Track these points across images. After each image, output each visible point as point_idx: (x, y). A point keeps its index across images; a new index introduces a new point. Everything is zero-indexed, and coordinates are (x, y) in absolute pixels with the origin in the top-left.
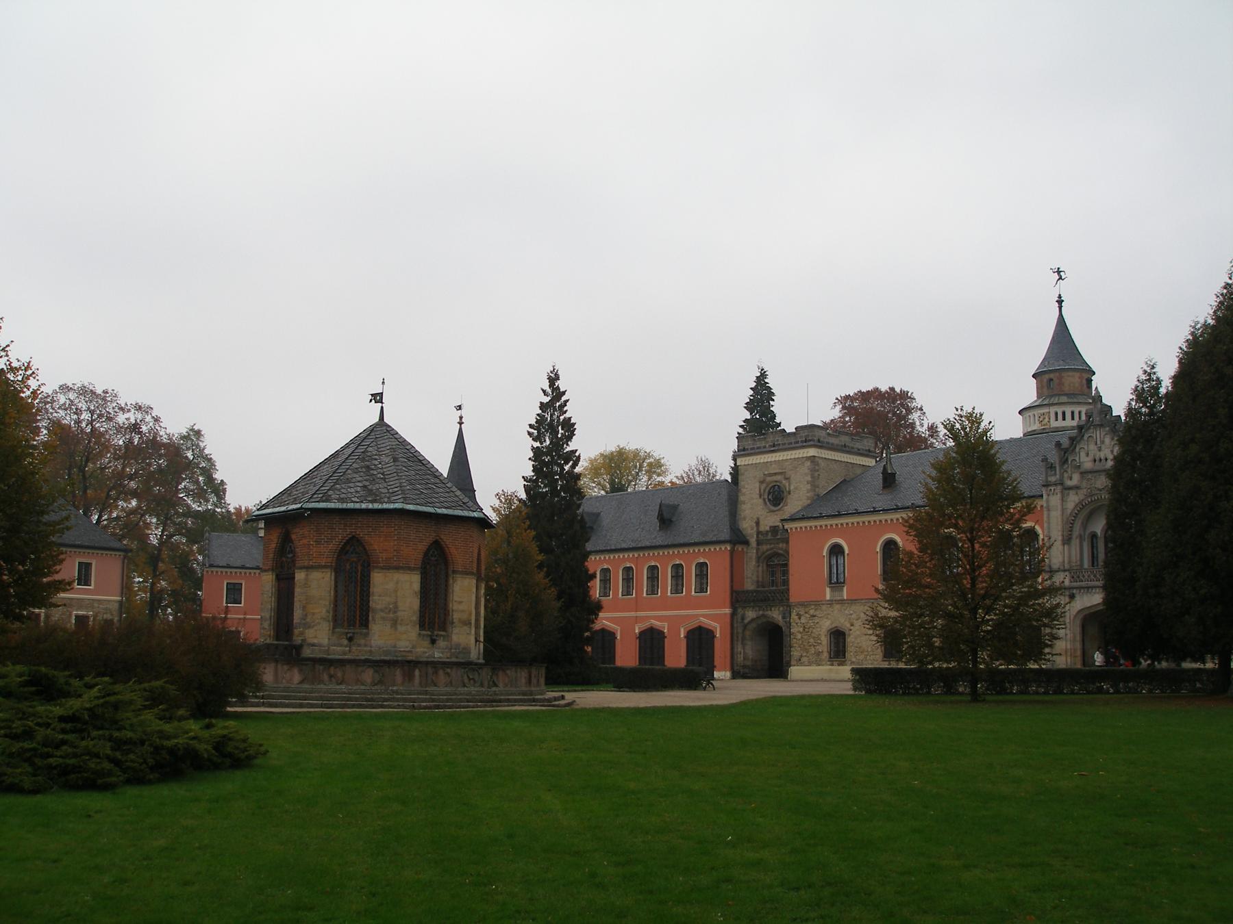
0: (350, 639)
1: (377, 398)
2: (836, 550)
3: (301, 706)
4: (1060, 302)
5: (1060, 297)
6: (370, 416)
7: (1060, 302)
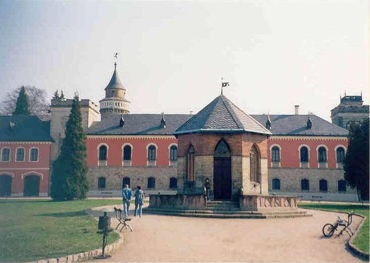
0: (255, 186)
2: (103, 148)
3: (204, 213)
4: (115, 65)
5: (116, 63)
7: (115, 65)
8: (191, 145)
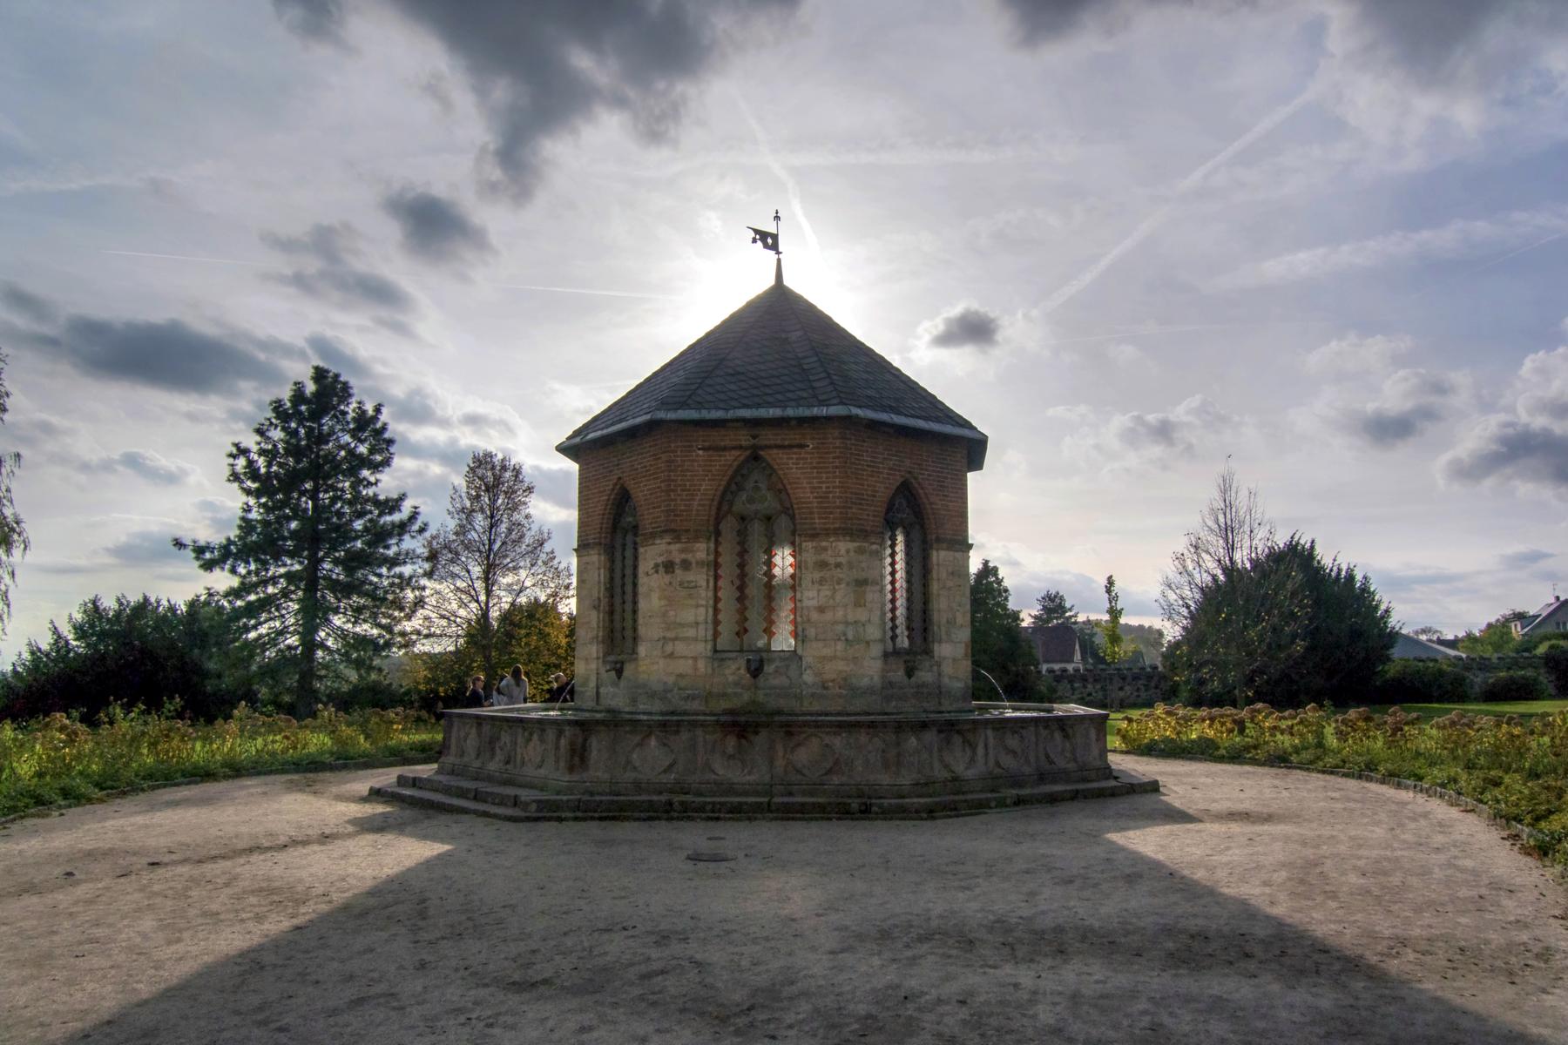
1: (768, 240)
8: (622, 500)
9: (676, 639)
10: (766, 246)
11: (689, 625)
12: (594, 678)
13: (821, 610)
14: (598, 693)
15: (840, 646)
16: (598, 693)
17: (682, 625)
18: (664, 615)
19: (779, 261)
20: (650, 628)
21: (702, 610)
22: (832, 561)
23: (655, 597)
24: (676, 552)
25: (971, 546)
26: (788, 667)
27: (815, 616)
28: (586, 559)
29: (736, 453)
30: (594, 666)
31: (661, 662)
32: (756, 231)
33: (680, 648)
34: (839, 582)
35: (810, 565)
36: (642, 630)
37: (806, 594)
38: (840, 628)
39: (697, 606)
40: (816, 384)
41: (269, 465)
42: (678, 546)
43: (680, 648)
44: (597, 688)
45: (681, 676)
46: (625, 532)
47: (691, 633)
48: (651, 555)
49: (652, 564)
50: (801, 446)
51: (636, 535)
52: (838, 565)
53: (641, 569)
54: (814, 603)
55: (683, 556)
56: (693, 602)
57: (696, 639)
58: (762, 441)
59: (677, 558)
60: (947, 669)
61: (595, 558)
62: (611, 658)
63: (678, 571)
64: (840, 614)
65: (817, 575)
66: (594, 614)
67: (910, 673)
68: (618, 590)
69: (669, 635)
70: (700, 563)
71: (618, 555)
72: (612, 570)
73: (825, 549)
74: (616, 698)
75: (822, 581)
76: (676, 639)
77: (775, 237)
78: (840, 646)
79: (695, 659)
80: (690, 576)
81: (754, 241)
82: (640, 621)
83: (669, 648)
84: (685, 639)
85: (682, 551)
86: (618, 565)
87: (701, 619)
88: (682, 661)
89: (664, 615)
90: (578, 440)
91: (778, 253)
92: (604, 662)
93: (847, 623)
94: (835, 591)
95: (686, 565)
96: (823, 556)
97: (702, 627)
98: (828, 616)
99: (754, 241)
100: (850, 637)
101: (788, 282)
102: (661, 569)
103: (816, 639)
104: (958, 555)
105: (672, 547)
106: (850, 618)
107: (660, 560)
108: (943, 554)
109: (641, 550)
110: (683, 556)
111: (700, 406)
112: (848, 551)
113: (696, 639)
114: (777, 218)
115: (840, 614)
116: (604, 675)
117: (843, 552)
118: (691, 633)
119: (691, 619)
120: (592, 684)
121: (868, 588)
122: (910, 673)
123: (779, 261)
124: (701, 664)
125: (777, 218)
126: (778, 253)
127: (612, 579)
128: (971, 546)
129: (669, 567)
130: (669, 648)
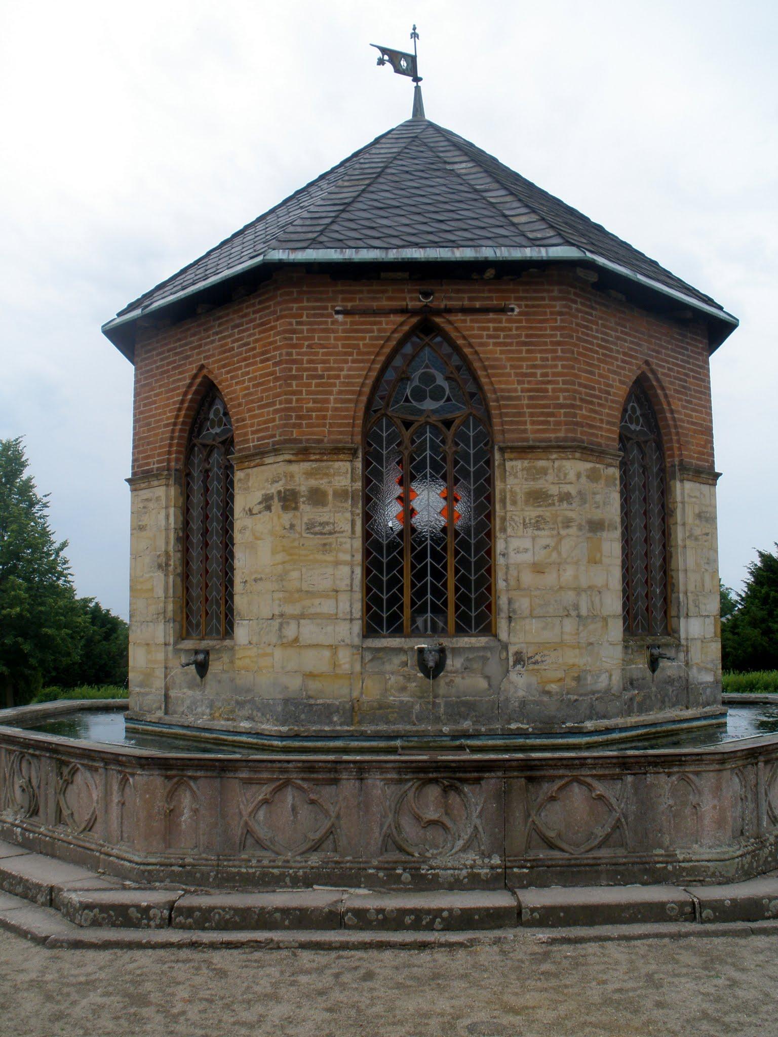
1: (404, 63)
6: (385, 107)
8: (206, 395)
9: (302, 616)
10: (398, 70)
11: (324, 595)
12: (160, 673)
13: (538, 569)
14: (167, 696)
15: (569, 625)
16: (167, 696)
17: (310, 594)
18: (281, 578)
19: (418, 90)
20: (253, 600)
21: (345, 570)
22: (554, 490)
23: (265, 549)
24: (300, 476)
25: (718, 475)
26: (485, 659)
27: (527, 578)
28: (145, 494)
29: (399, 319)
30: (160, 656)
31: (278, 653)
32: (384, 51)
33: (309, 632)
34: (567, 523)
35: (521, 497)
36: (240, 602)
37: (515, 543)
38: (570, 596)
39: (337, 563)
40: (515, 220)
41: (714, 913)
42: (306, 466)
43: (309, 632)
44: (167, 689)
45: (311, 675)
46: (211, 449)
47: (327, 606)
48: (252, 488)
49: (258, 496)
50: (503, 310)
51: (228, 452)
52: (566, 497)
53: (240, 503)
54: (527, 557)
55: (313, 483)
56: (329, 558)
57: (334, 618)
58: (439, 301)
59: (303, 485)
60: (696, 655)
61: (164, 495)
62: (189, 644)
63: (305, 508)
64: (568, 574)
65: (532, 513)
66: (160, 575)
67: (653, 664)
68: (196, 539)
69: (289, 610)
70: (342, 495)
71: (197, 486)
72: (186, 511)
73: (544, 472)
74: (199, 708)
75: (538, 524)
76: (302, 616)
77: (412, 60)
78: (569, 625)
79: (333, 648)
80: (324, 514)
81: (381, 62)
82: (238, 587)
83: (290, 632)
84: (313, 617)
85: (309, 474)
86: (197, 498)
87: (343, 585)
88: (310, 654)
89: (281, 578)
90: (137, 312)
91: (417, 79)
92: (177, 651)
93: (578, 590)
94: (560, 538)
95: (317, 497)
96: (540, 484)
97: (344, 598)
98: (550, 579)
99: (381, 62)
100: (584, 612)
101: (430, 115)
102: (276, 505)
103: (532, 616)
104: (705, 488)
105: (294, 468)
106: (584, 583)
107: (273, 489)
108: (688, 485)
109: (239, 475)
110: (313, 483)
111: (340, 244)
112: (578, 476)
113: (334, 618)
114: (415, 35)
115: (568, 574)
116: (177, 671)
117: (572, 476)
118: (327, 606)
119: (326, 585)
120: (159, 683)
121: (605, 534)
122: (653, 664)
123: (418, 90)
124: (345, 657)
125: (415, 35)
126: (417, 79)
127: (186, 524)
128: (718, 475)
129: (289, 500)
130: (290, 632)
